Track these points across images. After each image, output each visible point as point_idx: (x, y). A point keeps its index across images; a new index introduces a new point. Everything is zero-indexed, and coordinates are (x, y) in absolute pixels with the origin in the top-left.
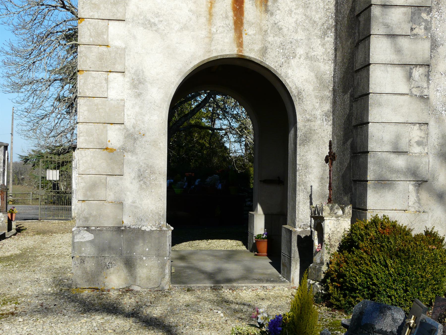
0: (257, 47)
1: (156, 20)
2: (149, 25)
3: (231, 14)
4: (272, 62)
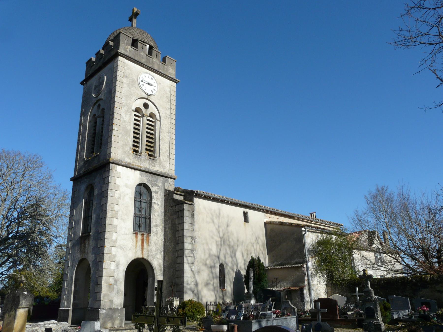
0: (147, 255)
1: (123, 247)
2: (122, 248)
3: (141, 246)
4: (150, 259)
